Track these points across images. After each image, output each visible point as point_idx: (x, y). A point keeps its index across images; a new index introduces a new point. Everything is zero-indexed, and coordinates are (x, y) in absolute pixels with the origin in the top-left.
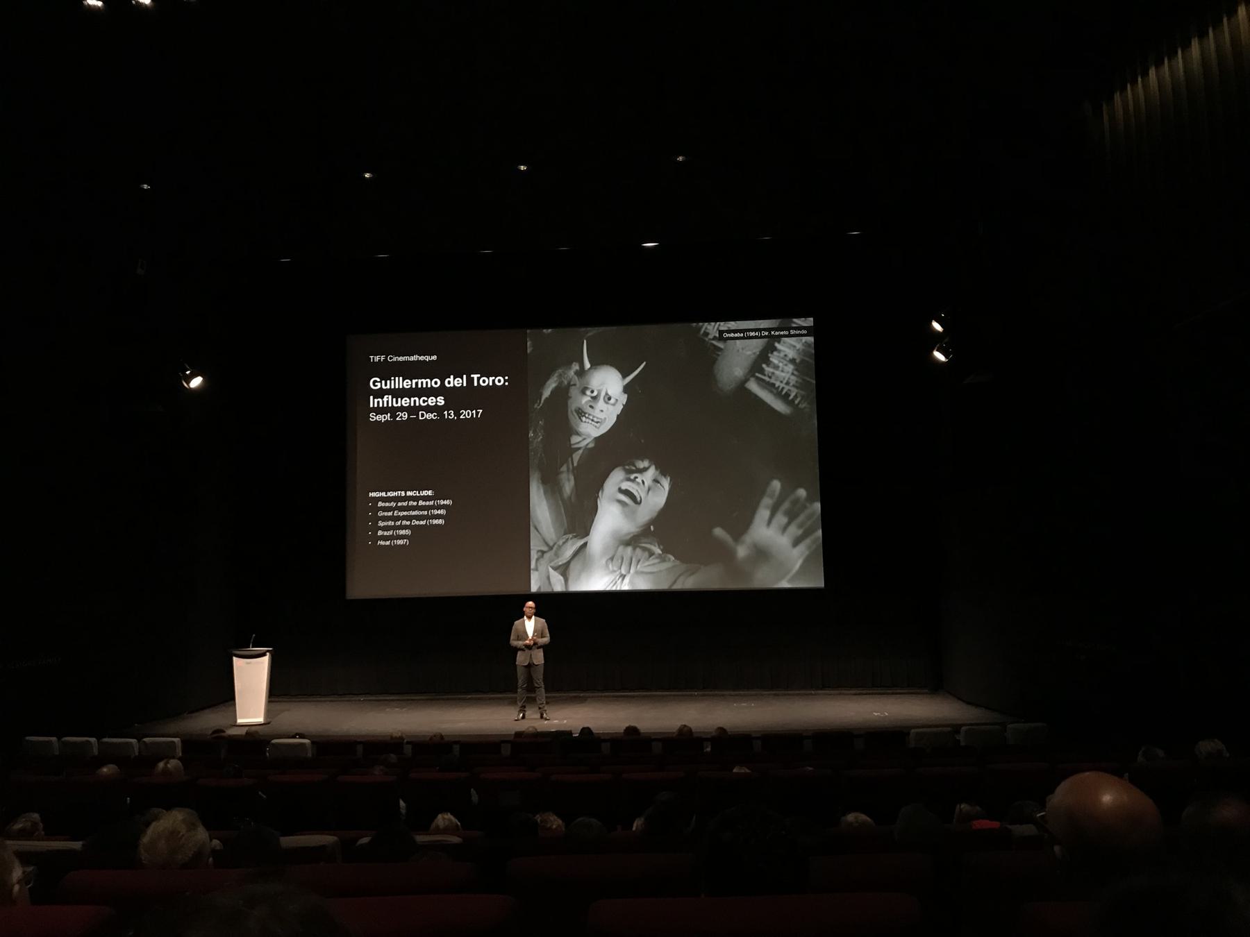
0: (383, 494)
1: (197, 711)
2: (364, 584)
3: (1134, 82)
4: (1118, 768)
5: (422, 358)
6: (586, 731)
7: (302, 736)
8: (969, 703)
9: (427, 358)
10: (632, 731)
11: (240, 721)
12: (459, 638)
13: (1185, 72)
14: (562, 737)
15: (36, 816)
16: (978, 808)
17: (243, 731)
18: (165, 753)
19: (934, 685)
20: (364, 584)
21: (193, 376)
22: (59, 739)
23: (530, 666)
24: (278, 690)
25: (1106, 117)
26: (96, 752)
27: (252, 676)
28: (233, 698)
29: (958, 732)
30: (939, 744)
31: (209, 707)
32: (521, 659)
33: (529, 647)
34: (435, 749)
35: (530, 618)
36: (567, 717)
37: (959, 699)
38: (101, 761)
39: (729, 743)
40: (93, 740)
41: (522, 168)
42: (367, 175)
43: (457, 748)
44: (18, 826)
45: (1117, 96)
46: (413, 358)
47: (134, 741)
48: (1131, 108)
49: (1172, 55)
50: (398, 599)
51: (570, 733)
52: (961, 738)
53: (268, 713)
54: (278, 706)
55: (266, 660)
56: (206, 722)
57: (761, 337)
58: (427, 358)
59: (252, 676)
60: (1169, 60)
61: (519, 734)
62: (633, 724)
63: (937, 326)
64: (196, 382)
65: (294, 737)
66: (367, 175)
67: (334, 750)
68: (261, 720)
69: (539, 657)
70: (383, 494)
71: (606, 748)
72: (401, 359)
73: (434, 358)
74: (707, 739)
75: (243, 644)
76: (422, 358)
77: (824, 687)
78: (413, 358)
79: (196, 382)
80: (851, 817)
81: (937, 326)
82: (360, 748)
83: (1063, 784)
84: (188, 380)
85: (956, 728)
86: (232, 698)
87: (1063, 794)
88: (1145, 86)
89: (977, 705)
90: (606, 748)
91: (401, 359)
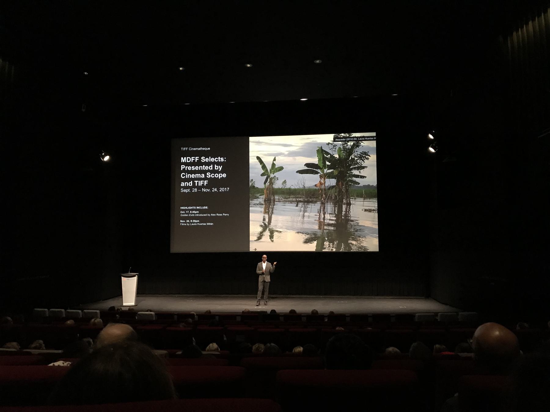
0: (186, 208)
1: (107, 299)
2: (179, 246)
3: (522, 28)
4: (318, 64)
5: (204, 149)
6: (273, 311)
7: (151, 311)
8: (443, 304)
9: (206, 149)
10: (293, 312)
11: (124, 304)
12: (237, 268)
13: (546, 24)
14: (263, 314)
15: (41, 341)
16: (444, 347)
17: (127, 309)
18: (94, 316)
19: (427, 295)
20: (179, 246)
21: (106, 155)
22: (49, 310)
23: (264, 282)
24: (141, 291)
25: (509, 42)
26: (64, 316)
27: (130, 285)
28: (122, 295)
29: (437, 316)
30: (429, 319)
31: (116, 296)
32: (261, 279)
33: (263, 274)
34: (207, 316)
35: (264, 262)
36: (282, 306)
37: (439, 302)
38: (67, 319)
39: (335, 318)
40: (63, 310)
41: (248, 65)
42: (181, 69)
43: (217, 318)
44: (33, 345)
45: (515, 33)
46: (199, 149)
47: (80, 311)
48: (521, 40)
49: (539, 16)
50: (202, 253)
51: (266, 312)
52: (438, 318)
53: (136, 301)
54: (141, 298)
55: (135, 279)
56: (111, 303)
57: (354, 141)
58: (206, 149)
59: (130, 285)
60: (538, 18)
61: (243, 312)
62: (290, 309)
63: (431, 137)
64: (107, 158)
65: (147, 311)
66: (181, 69)
67: (165, 317)
68: (133, 304)
69: (268, 279)
70: (186, 208)
71: (282, 319)
72: (195, 149)
73: (209, 149)
74: (326, 316)
75: (126, 271)
76: (204, 149)
77: (377, 295)
78: (199, 149)
79: (107, 158)
80: (391, 349)
81: (431, 137)
82: (176, 317)
83: (480, 328)
84: (103, 157)
85: (436, 314)
86: (121, 295)
87: (478, 331)
88: (527, 30)
89: (446, 304)
90: (282, 319)
91: (195, 149)
